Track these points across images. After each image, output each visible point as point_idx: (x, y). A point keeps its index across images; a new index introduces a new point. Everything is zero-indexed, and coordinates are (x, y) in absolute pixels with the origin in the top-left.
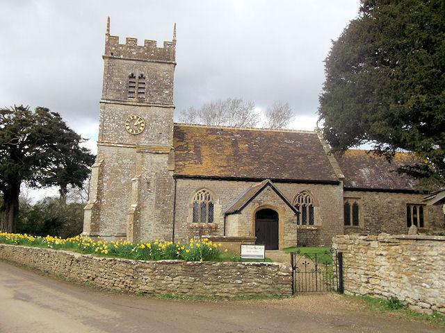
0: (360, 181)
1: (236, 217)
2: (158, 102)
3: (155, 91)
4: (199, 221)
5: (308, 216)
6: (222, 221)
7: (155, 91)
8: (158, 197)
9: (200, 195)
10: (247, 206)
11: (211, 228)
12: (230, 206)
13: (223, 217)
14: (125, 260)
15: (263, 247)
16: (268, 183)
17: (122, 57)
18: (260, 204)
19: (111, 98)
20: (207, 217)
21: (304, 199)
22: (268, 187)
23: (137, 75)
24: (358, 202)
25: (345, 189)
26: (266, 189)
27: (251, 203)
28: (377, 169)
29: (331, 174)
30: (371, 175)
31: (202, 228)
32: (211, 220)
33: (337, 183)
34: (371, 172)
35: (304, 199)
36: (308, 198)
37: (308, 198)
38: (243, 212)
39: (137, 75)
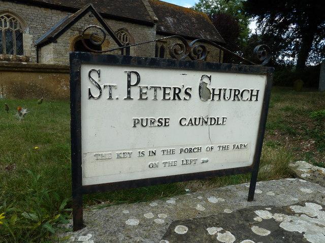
0: (167, 27)
1: (51, 47)
4: (5, 51)
6: (34, 54)
10: (65, 34)
12: (44, 35)
14: (106, 53)
15: (280, 226)
16: (90, 8)
18: (80, 32)
20: (15, 48)
21: (122, 37)
22: (90, 13)
24: (165, 45)
25: (159, 33)
26: (87, 16)
27: (69, 32)
28: (178, 19)
29: (146, 15)
30: (174, 23)
32: (21, 51)
33: (150, 25)
34: (174, 21)
35: (122, 37)
36: (125, 36)
37: (125, 36)
38: (59, 40)
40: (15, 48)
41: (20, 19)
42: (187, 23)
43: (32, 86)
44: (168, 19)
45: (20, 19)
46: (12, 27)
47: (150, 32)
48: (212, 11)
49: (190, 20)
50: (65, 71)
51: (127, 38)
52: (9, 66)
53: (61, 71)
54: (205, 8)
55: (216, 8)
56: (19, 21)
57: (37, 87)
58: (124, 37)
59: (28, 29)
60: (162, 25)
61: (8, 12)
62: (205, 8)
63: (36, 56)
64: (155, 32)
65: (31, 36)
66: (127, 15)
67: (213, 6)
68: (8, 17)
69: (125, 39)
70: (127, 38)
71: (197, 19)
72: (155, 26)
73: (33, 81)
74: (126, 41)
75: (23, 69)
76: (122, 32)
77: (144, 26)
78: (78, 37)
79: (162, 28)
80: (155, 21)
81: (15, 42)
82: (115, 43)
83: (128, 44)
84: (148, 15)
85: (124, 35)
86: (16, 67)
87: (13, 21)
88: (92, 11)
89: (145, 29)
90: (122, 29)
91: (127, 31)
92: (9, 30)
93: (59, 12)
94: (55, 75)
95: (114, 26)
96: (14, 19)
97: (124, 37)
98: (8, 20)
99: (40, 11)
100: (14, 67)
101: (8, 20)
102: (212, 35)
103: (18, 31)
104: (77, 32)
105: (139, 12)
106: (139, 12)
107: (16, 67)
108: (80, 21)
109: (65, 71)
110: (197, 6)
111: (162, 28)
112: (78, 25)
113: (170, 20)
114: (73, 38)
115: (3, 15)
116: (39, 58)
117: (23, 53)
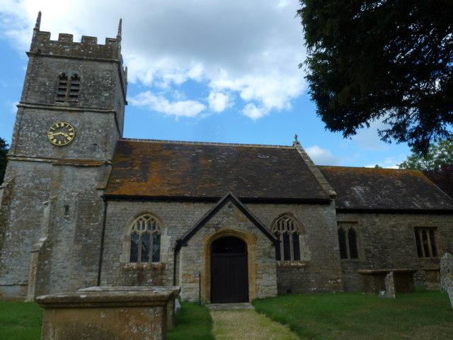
0: (354, 200)
2: (94, 106)
3: (90, 94)
5: (292, 248)
6: (171, 260)
7: (90, 94)
8: (79, 227)
9: (141, 223)
11: (155, 269)
12: (182, 232)
13: (172, 253)
17: (51, 54)
19: (33, 101)
21: (286, 225)
22: (229, 203)
23: (70, 74)
24: (354, 227)
26: (225, 208)
27: (203, 229)
31: (141, 269)
32: (297, 257)
33: (325, 202)
34: (365, 190)
35: (286, 225)
37: (290, 223)
38: (190, 242)
39: (70, 74)
40: (150, 255)
41: (160, 219)
42: (387, 189)
43: (91, 328)
44: (355, 189)
45: (160, 219)
46: (150, 229)
47: (325, 212)
48: (437, 162)
49: (393, 184)
50: (134, 304)
51: (293, 225)
52: (65, 301)
53: (130, 304)
54: (424, 160)
55: (442, 156)
56: (158, 221)
57: (96, 329)
58: (288, 225)
59: (166, 229)
60: (346, 199)
61: (146, 213)
62: (424, 160)
63: (173, 262)
64: (334, 212)
65: (170, 237)
66: (294, 196)
67: (436, 156)
68: (147, 218)
69: (281, 227)
70: (293, 225)
71: (404, 182)
72: (333, 203)
73: (93, 320)
74: (293, 229)
75: (81, 305)
76: (285, 218)
77: (317, 205)
78: (214, 236)
79: (347, 203)
80: (333, 196)
81: (151, 246)
82: (266, 238)
83: (295, 233)
84: (322, 189)
85: (288, 222)
86: (73, 303)
87: (152, 222)
88: (232, 201)
89: (318, 209)
90: (284, 214)
91: (292, 215)
92: (146, 233)
93: (202, 204)
94: (122, 311)
95: (267, 214)
96: (153, 220)
97: (288, 225)
98: (146, 221)
99: (181, 207)
100: (69, 303)
101: (146, 221)
102: (435, 200)
103: (156, 232)
104: (214, 229)
105: (307, 188)
106: (307, 188)
107: (73, 303)
108: (217, 214)
109: (134, 304)
110: (410, 159)
111: (347, 203)
112: (214, 220)
113: (358, 190)
114: (208, 237)
115: (141, 217)
116: (177, 264)
117: (159, 258)
